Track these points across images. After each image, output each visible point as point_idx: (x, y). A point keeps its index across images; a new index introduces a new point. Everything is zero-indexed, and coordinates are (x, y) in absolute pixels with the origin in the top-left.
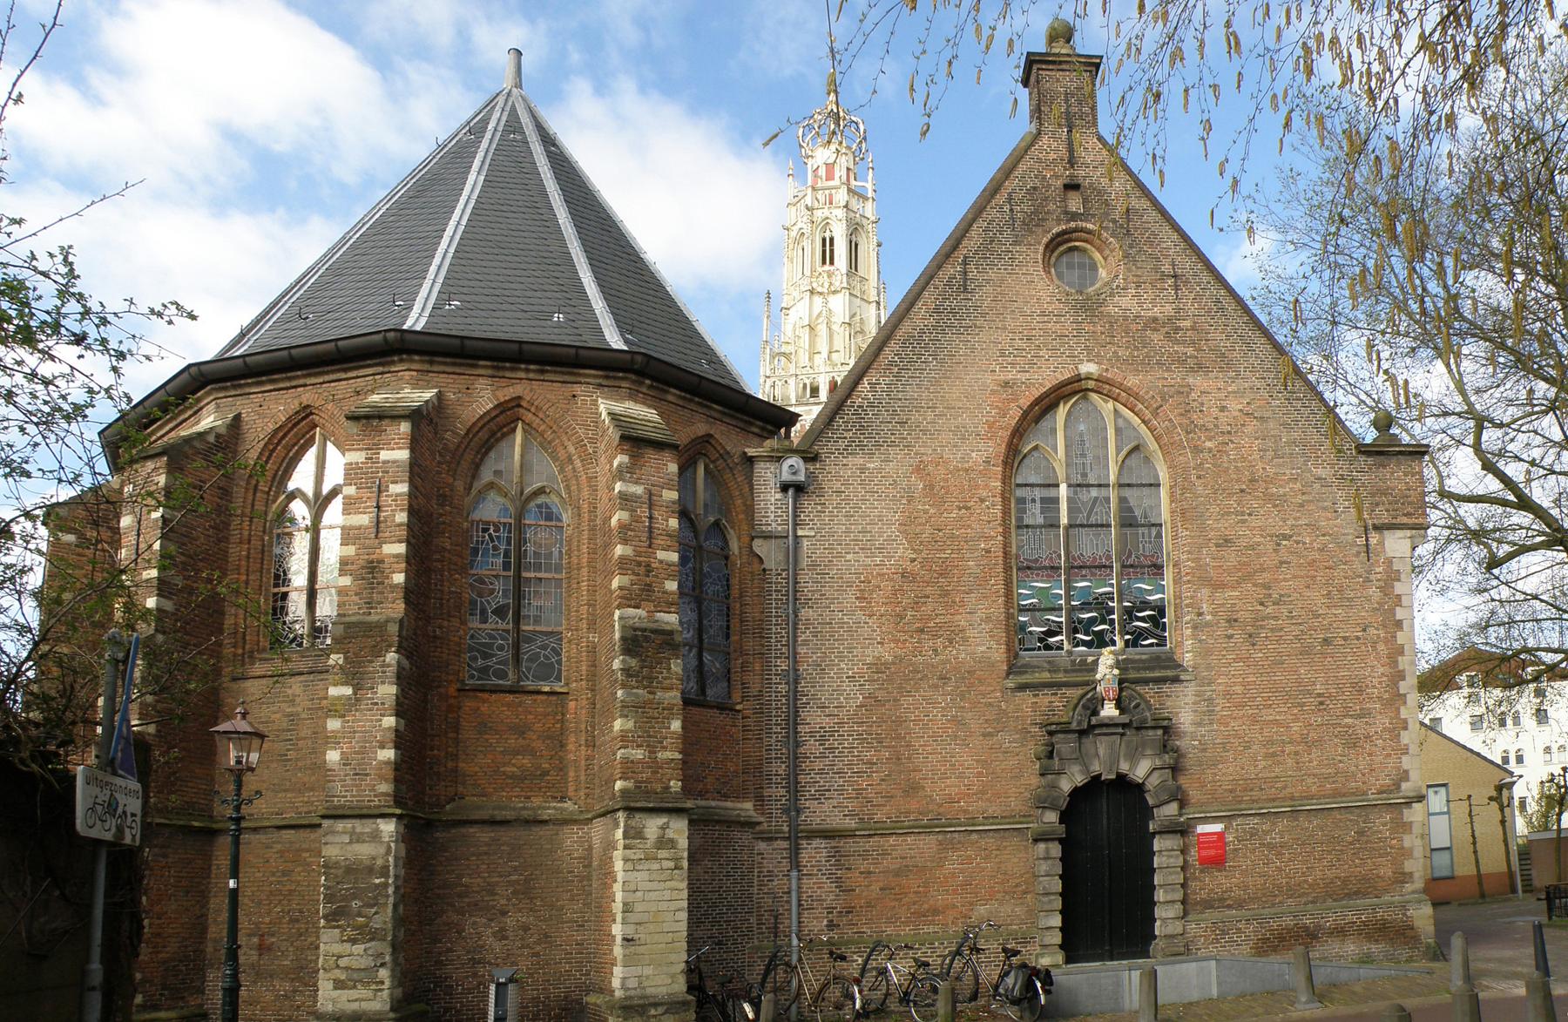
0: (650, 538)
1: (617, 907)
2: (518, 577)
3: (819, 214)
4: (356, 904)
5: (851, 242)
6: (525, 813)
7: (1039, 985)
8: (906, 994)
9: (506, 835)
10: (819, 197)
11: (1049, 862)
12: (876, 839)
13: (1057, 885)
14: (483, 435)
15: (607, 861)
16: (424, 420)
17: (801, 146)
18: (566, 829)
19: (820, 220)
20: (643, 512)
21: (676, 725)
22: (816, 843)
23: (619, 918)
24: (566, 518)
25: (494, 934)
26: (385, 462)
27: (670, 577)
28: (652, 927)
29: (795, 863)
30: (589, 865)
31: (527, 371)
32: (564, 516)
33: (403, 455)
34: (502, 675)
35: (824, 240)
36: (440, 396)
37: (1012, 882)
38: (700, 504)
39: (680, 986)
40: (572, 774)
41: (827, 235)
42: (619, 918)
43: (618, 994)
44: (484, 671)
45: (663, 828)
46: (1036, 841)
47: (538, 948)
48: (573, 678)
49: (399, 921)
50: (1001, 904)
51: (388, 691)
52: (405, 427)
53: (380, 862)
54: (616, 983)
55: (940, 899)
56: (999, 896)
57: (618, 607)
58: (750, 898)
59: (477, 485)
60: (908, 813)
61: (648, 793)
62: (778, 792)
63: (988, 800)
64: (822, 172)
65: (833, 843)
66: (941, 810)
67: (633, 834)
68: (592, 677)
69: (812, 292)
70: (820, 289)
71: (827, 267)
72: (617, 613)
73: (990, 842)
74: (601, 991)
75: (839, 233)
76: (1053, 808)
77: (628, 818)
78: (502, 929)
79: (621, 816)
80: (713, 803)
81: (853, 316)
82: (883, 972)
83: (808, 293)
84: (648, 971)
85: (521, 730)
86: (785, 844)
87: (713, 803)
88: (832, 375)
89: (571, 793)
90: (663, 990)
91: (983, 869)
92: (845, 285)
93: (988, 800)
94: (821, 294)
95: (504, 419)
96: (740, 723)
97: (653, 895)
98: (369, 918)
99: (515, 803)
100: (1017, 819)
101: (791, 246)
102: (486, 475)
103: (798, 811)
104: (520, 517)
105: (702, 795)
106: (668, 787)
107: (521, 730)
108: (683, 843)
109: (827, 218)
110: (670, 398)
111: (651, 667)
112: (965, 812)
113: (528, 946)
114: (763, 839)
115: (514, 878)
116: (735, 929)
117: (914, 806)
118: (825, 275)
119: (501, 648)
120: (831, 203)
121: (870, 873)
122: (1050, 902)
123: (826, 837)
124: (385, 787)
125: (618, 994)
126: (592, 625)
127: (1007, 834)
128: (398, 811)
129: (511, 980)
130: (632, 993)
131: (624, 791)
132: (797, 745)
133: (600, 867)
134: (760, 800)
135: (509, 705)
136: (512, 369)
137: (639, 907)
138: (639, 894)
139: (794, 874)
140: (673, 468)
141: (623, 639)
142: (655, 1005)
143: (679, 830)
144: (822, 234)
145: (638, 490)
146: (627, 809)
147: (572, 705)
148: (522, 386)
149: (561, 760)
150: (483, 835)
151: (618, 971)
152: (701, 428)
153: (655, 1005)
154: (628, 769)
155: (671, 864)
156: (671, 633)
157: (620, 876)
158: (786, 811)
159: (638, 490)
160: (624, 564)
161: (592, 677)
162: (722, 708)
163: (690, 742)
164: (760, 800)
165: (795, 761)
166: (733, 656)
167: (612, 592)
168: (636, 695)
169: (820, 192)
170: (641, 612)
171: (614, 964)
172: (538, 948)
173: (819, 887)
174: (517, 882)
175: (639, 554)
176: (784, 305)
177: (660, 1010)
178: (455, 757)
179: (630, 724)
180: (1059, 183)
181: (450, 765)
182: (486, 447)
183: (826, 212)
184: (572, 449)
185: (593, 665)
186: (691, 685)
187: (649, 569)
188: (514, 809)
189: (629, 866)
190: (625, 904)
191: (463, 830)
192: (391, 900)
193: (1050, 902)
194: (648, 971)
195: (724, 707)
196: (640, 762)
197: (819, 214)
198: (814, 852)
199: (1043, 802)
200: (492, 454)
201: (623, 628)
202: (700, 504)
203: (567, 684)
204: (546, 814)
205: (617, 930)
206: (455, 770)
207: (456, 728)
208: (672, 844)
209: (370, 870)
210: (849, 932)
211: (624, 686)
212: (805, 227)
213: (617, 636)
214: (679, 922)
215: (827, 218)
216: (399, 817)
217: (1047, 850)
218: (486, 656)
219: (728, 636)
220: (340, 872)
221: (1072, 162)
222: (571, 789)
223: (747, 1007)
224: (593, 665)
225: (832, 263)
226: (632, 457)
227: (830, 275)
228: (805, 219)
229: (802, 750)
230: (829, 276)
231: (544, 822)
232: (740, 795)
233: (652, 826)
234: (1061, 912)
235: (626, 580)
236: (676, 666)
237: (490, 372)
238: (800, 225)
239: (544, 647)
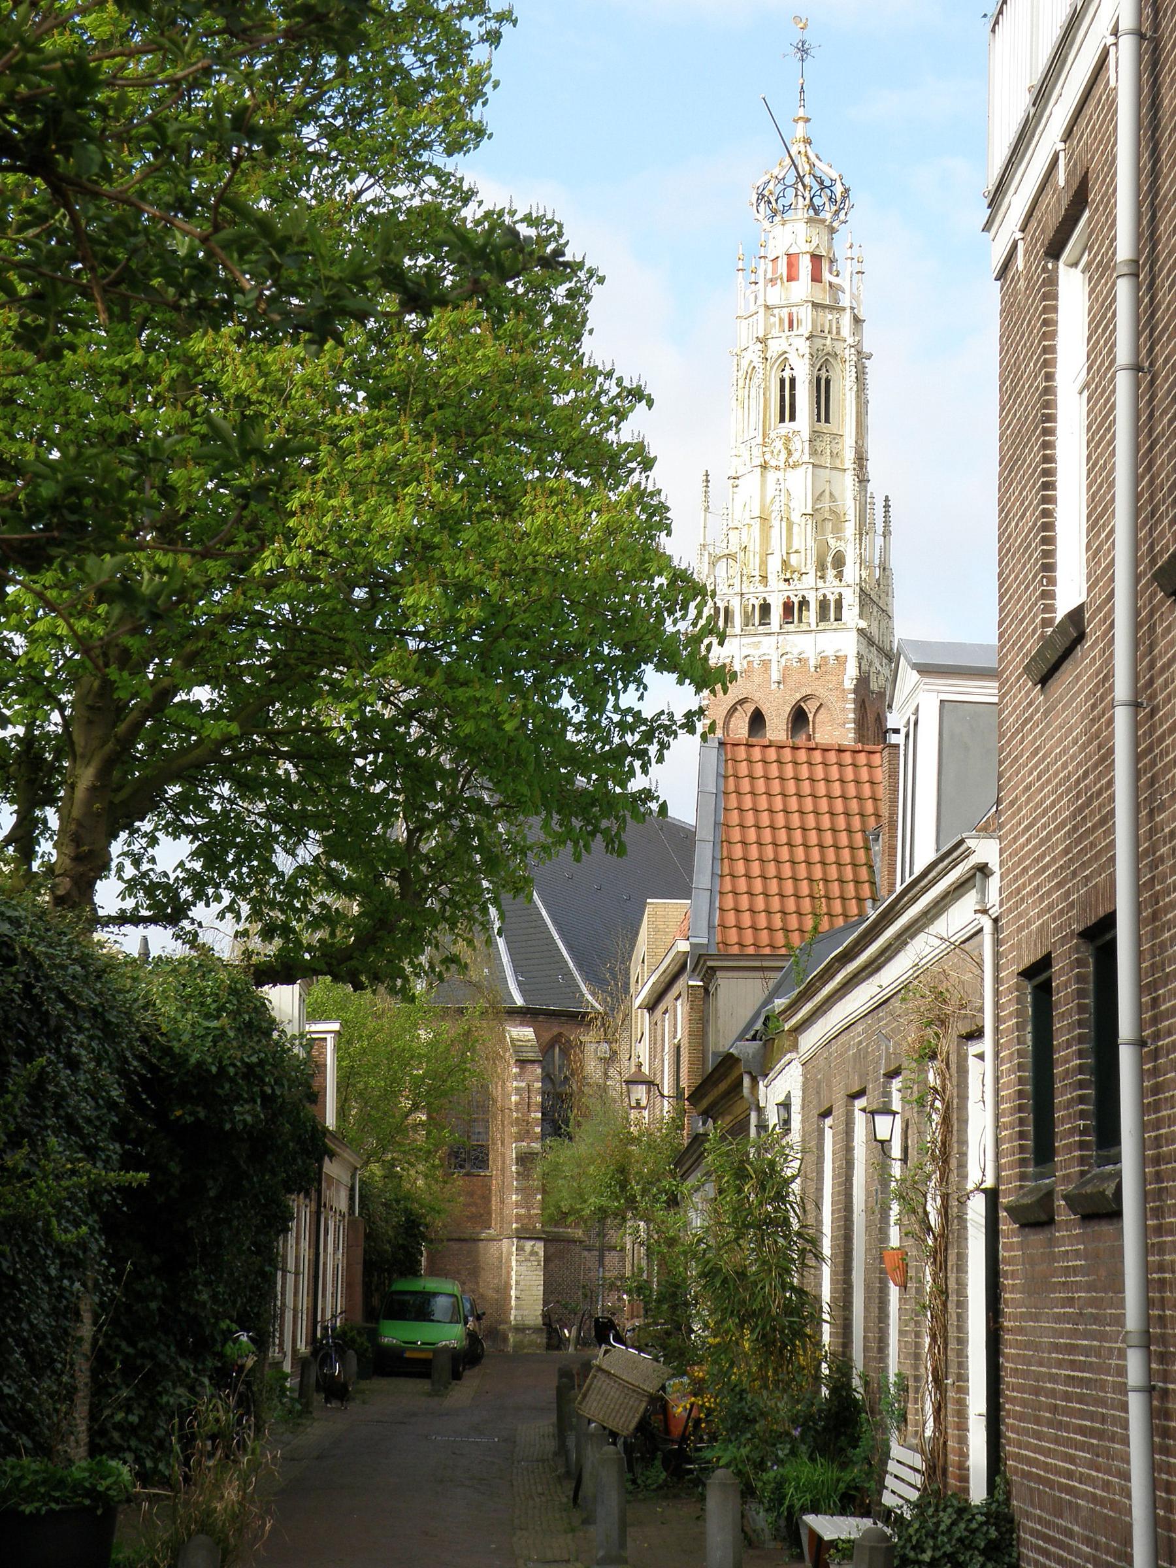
1: (513, 1282)
5: (819, 380)
15: (509, 1261)
19: (775, 355)
20: (525, 1095)
21: (539, 1197)
29: (601, 1263)
35: (782, 381)
39: (540, 1321)
41: (787, 374)
48: (494, 1171)
67: (520, 1249)
69: (764, 467)
81: (818, 498)
101: (741, 383)
108: (542, 1253)
140: (539, 1071)
143: (540, 1247)
145: (523, 1085)
152: (555, 1031)
154: (518, 1218)
159: (523, 1085)
197: (775, 347)
204: (483, 1236)
205: (513, 1293)
208: (537, 1254)
225: (792, 418)
233: (528, 1245)
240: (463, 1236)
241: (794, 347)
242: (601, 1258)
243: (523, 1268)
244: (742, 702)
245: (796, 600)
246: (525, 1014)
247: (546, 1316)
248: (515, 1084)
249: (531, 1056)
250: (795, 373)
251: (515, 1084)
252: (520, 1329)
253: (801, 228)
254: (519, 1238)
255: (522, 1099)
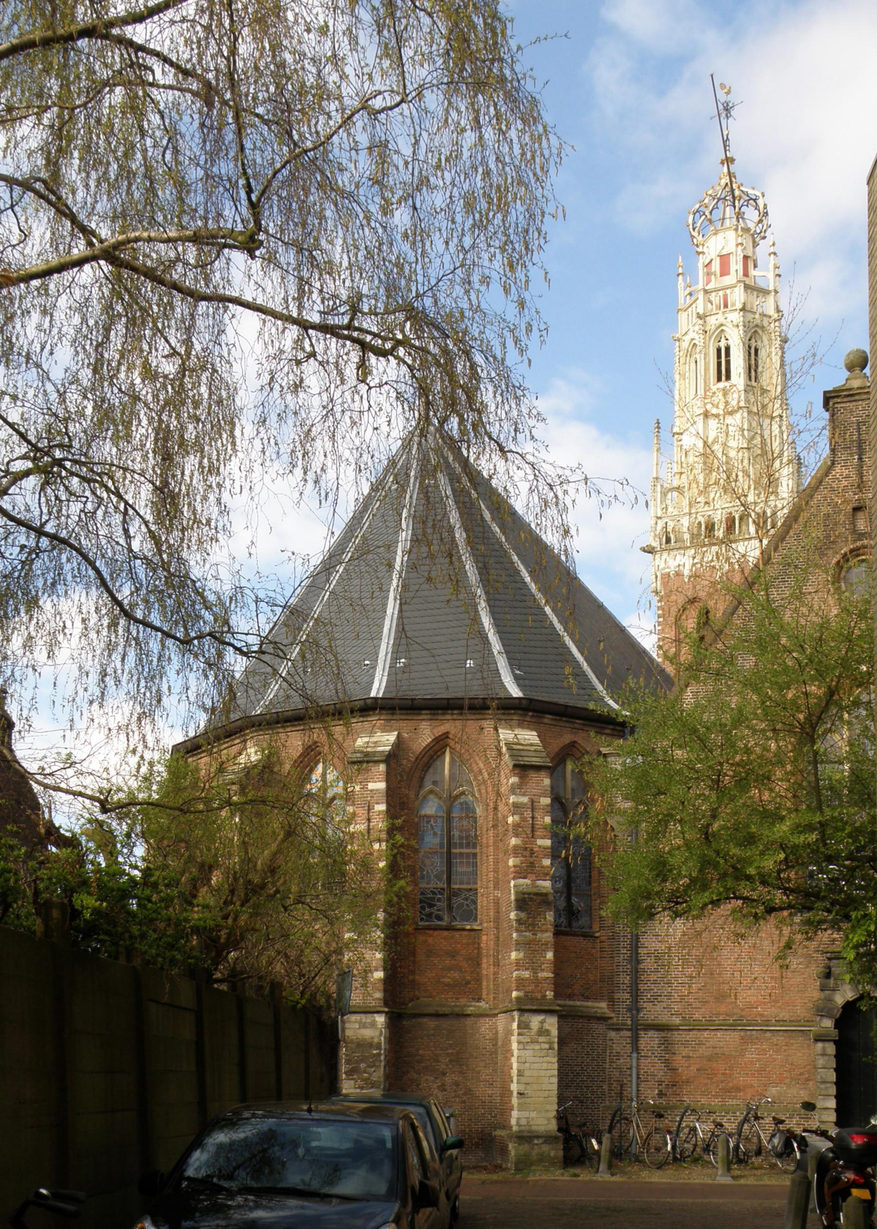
0: (533, 831)
1: (514, 1072)
2: (449, 853)
3: (712, 321)
4: (363, 1066)
5: (750, 347)
6: (457, 1010)
7: (795, 1145)
8: (708, 1146)
9: (445, 1023)
10: (712, 299)
11: (826, 1058)
12: (694, 1032)
13: (832, 1076)
14: (425, 759)
15: (507, 1043)
16: (392, 758)
17: (692, 237)
18: (482, 1020)
19: (713, 328)
20: (528, 814)
21: (550, 955)
22: (651, 1033)
23: (515, 1079)
24: (479, 811)
25: (438, 1087)
26: (372, 791)
27: (545, 857)
28: (535, 1087)
29: (636, 1048)
30: (495, 1045)
31: (452, 714)
32: (478, 811)
33: (382, 785)
34: (439, 918)
35: (719, 350)
36: (399, 737)
37: (797, 1072)
38: (569, 790)
39: (553, 1126)
40: (484, 983)
41: (723, 344)
42: (515, 1079)
43: (515, 1128)
44: (430, 915)
45: (542, 1022)
46: (817, 1040)
47: (465, 1098)
48: (484, 921)
49: (387, 1077)
50: (789, 1087)
51: (378, 935)
52: (382, 767)
53: (376, 1040)
54: (513, 1122)
55: (742, 1080)
56: (787, 1081)
57: (514, 878)
58: (604, 1071)
59: (422, 792)
60: (718, 1014)
61: (532, 1000)
62: (624, 996)
63: (780, 1007)
64: (716, 267)
65: (663, 1034)
66: (744, 1013)
68: (497, 920)
70: (714, 411)
71: (721, 385)
72: (512, 883)
73: (780, 1039)
74: (504, 1127)
75: (735, 340)
76: (829, 1016)
77: (520, 1016)
78: (443, 1085)
79: (516, 1014)
80: (578, 1003)
82: (694, 1129)
83: (702, 417)
84: (533, 1115)
85: (453, 955)
86: (629, 1034)
87: (578, 1003)
89: (484, 996)
90: (542, 1128)
91: (775, 1060)
92: (742, 404)
93: (780, 1007)
94: (717, 416)
95: (440, 744)
96: (598, 946)
97: (536, 1066)
98: (370, 1074)
99: (450, 1002)
100: (802, 1023)
102: (428, 786)
103: (638, 1010)
104: (449, 813)
105: (570, 997)
106: (545, 996)
107: (453, 955)
108: (555, 1032)
109: (722, 325)
110: (546, 721)
111: (534, 918)
112: (762, 1015)
113: (458, 1096)
114: (613, 1030)
115: (450, 1051)
116: (593, 1092)
117: (723, 1009)
118: (720, 395)
119: (439, 900)
120: (726, 306)
121: (689, 1057)
122: (826, 1088)
123: (658, 1030)
124: (379, 995)
125: (515, 1128)
126: (496, 886)
127: (794, 1034)
128: (386, 1010)
129: (452, 1115)
130: (523, 1128)
131: (518, 999)
132: (638, 962)
133: (503, 1046)
134: (612, 1001)
135: (445, 938)
136: (443, 714)
137: (527, 1073)
138: (527, 1065)
139: (635, 1055)
140: (547, 782)
141: (517, 900)
142: (538, 1137)
143: (552, 1023)
144: (717, 344)
145: (525, 800)
146: (520, 1010)
147: (484, 938)
148: (449, 725)
149: (478, 974)
150: (431, 1023)
151: (515, 1114)
152: (567, 738)
153: (538, 1137)
154: (520, 983)
155: (547, 1046)
156: (546, 895)
157: (516, 1053)
158: (630, 1010)
159: (525, 800)
160: (516, 851)
161: (497, 920)
162: (585, 935)
163: (558, 965)
164: (612, 1001)
165: (636, 974)
166: (594, 897)
167: (509, 868)
168: (525, 936)
169: (713, 294)
170: (527, 881)
171: (512, 1109)
172: (465, 1098)
173: (652, 1066)
174: (452, 1054)
175: (525, 843)
176: (676, 430)
177: (541, 1141)
178: (413, 972)
179: (521, 955)
180: (849, 508)
181: (411, 977)
182: (428, 766)
183: (720, 318)
184: (481, 765)
185: (498, 912)
186: (562, 919)
187: (532, 852)
188: (450, 1006)
189: (521, 1046)
190: (519, 1071)
191: (420, 1020)
192: (383, 1064)
193: (826, 1088)
194: (533, 1115)
195: (588, 935)
196: (527, 979)
197: (712, 321)
198: (649, 1040)
199: (822, 1011)
200: (431, 770)
201: (516, 893)
202: (569, 790)
203: (481, 924)
204: (470, 1010)
205: (514, 1087)
206: (413, 981)
207: (414, 954)
208: (547, 1033)
209: (371, 1045)
210: (674, 1100)
211: (517, 931)
212: (697, 337)
213: (513, 897)
214: (552, 1084)
215: (722, 325)
216: (386, 1013)
217: (824, 1049)
218: (431, 906)
219: (590, 883)
220: (353, 1046)
221: (861, 486)
222: (484, 993)
223: (594, 1142)
224: (498, 912)
225: (728, 377)
226: (521, 778)
227: (725, 392)
228: (697, 328)
229: (641, 966)
230: (725, 395)
231: (469, 1015)
232: (597, 998)
233: (535, 1021)
234: (836, 1097)
235: (518, 861)
236: (550, 916)
237: (429, 717)
238: (691, 335)
239: (466, 899)
240: (442, 1010)
241: (729, 320)
242: (635, 1040)
243: (528, 1053)
244: (693, 601)
246: (526, 709)
247: (562, 1118)
248: (512, 799)
249: (536, 761)
250: (730, 342)
251: (512, 799)
252: (525, 1137)
253: (731, 235)
254: (522, 1011)
255: (523, 819)
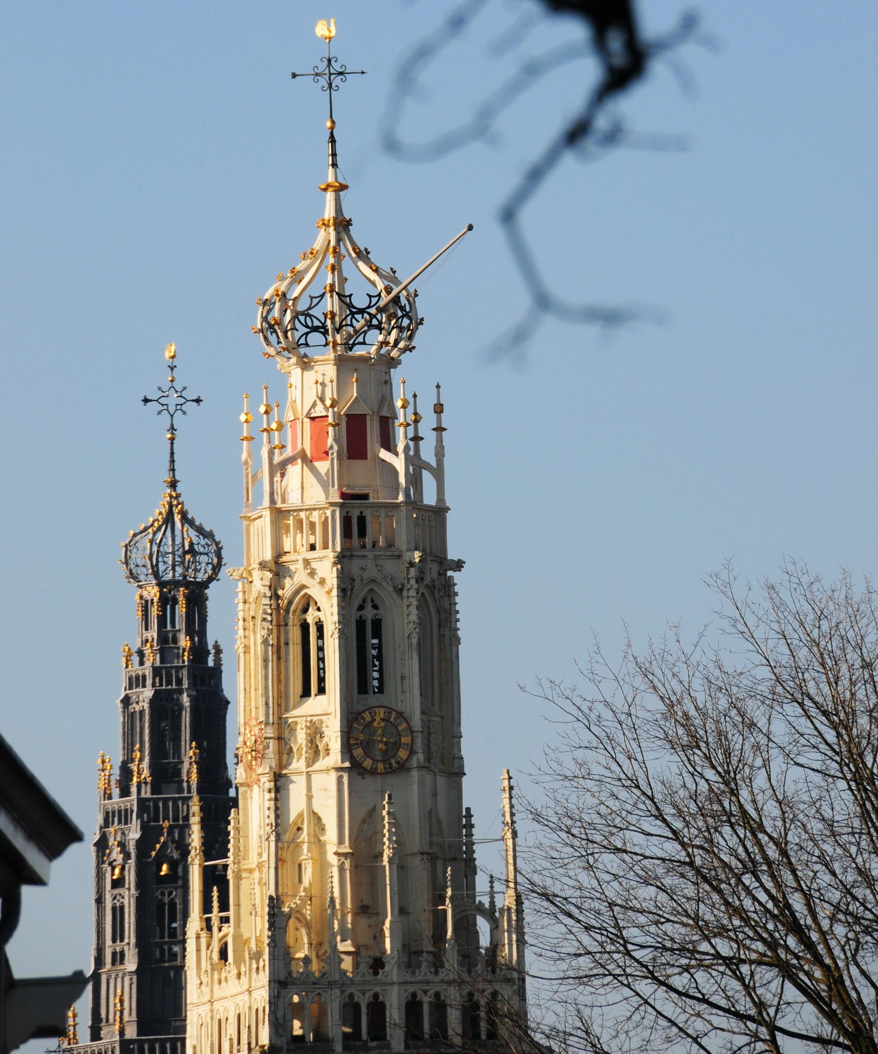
5: (361, 624)
88: (411, 989)
225: (322, 690)
245: (426, 1000)
